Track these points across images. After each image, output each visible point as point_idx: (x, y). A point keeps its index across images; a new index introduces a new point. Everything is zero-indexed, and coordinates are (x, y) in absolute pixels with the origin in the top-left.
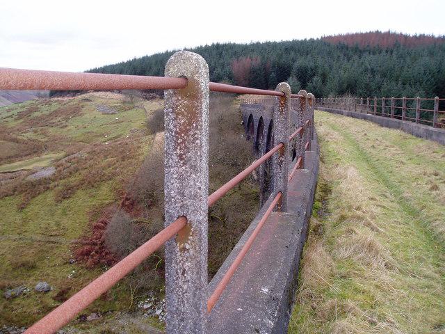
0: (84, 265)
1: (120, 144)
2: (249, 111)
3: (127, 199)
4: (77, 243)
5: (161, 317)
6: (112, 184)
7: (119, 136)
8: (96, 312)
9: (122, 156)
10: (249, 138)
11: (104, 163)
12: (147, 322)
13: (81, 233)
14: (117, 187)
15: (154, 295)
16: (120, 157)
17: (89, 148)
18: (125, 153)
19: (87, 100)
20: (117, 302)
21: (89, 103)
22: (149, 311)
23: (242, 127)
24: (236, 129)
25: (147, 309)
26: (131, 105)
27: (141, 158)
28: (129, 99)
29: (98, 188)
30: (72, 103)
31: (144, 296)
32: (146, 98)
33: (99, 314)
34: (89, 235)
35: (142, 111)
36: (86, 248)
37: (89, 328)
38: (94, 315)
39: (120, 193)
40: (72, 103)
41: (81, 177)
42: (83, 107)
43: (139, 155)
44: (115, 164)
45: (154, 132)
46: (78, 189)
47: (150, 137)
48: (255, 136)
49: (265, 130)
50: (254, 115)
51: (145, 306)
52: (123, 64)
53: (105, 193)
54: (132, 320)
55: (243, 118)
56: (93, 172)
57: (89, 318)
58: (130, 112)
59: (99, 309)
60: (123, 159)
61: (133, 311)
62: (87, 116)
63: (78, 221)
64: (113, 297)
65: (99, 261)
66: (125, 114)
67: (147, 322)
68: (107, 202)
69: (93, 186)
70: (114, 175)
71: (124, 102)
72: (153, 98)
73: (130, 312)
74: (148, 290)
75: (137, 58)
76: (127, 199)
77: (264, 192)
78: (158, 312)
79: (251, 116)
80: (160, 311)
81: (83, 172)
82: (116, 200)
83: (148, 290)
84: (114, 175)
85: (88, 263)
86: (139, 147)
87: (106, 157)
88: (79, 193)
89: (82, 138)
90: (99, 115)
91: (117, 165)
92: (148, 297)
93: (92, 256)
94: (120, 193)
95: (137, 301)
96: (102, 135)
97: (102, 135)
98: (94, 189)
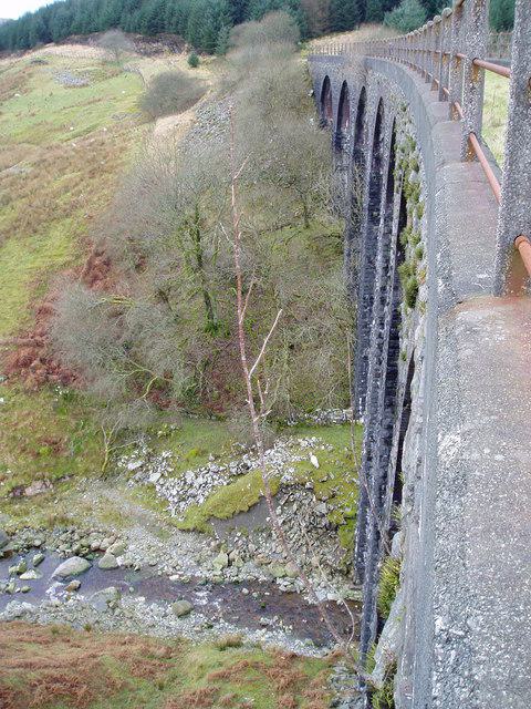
0: (21, 387)
1: (91, 144)
2: (324, 68)
3: (97, 254)
4: (7, 344)
5: (158, 487)
6: (71, 224)
7: (94, 127)
8: (42, 478)
9: (90, 168)
10: (323, 124)
11: (57, 185)
12: (135, 498)
13: (14, 323)
14: (78, 232)
15: (147, 441)
16: (88, 170)
17: (36, 153)
18: (97, 164)
19: (39, 62)
20: (79, 459)
21: (41, 68)
22: (138, 475)
23: (311, 102)
24: (297, 108)
25: (134, 472)
26: (118, 68)
27: (126, 169)
28: (112, 57)
29: (46, 231)
30: (12, 71)
31: (129, 444)
32: (147, 54)
33: (48, 483)
34: (30, 326)
35: (135, 77)
36: (24, 353)
37: (27, 513)
38: (38, 484)
39: (85, 242)
40: (12, 71)
41: (14, 214)
42: (30, 75)
43: (123, 164)
44: (77, 185)
45: (153, 119)
46: (8, 238)
47: (146, 127)
48: (333, 120)
49: (353, 109)
50: (331, 79)
51: (132, 466)
52: (46, 14)
53: (58, 244)
54: (106, 492)
55: (312, 85)
56: (37, 202)
57: (29, 491)
58: (112, 81)
59: (47, 474)
60: (92, 174)
61: (109, 475)
62: (37, 92)
63: (9, 301)
64: (72, 448)
65: (47, 379)
66: (104, 85)
67: (135, 498)
68: (61, 260)
69: (35, 232)
70: (75, 206)
71: (104, 63)
72: (158, 52)
73: (104, 477)
74: (135, 433)
75: (33, 12)
76: (97, 254)
77: (351, 237)
78: (154, 477)
79: (327, 80)
80: (158, 475)
81: (19, 204)
82: (78, 257)
83: (135, 433)
84: (75, 206)
85: (28, 383)
86: (122, 150)
87: (62, 171)
88: (12, 245)
89: (27, 136)
90: (59, 90)
91: (80, 187)
92: (136, 446)
93: (35, 369)
94: (85, 242)
95: (115, 455)
96: (63, 128)
97: (63, 128)
98: (37, 237)
